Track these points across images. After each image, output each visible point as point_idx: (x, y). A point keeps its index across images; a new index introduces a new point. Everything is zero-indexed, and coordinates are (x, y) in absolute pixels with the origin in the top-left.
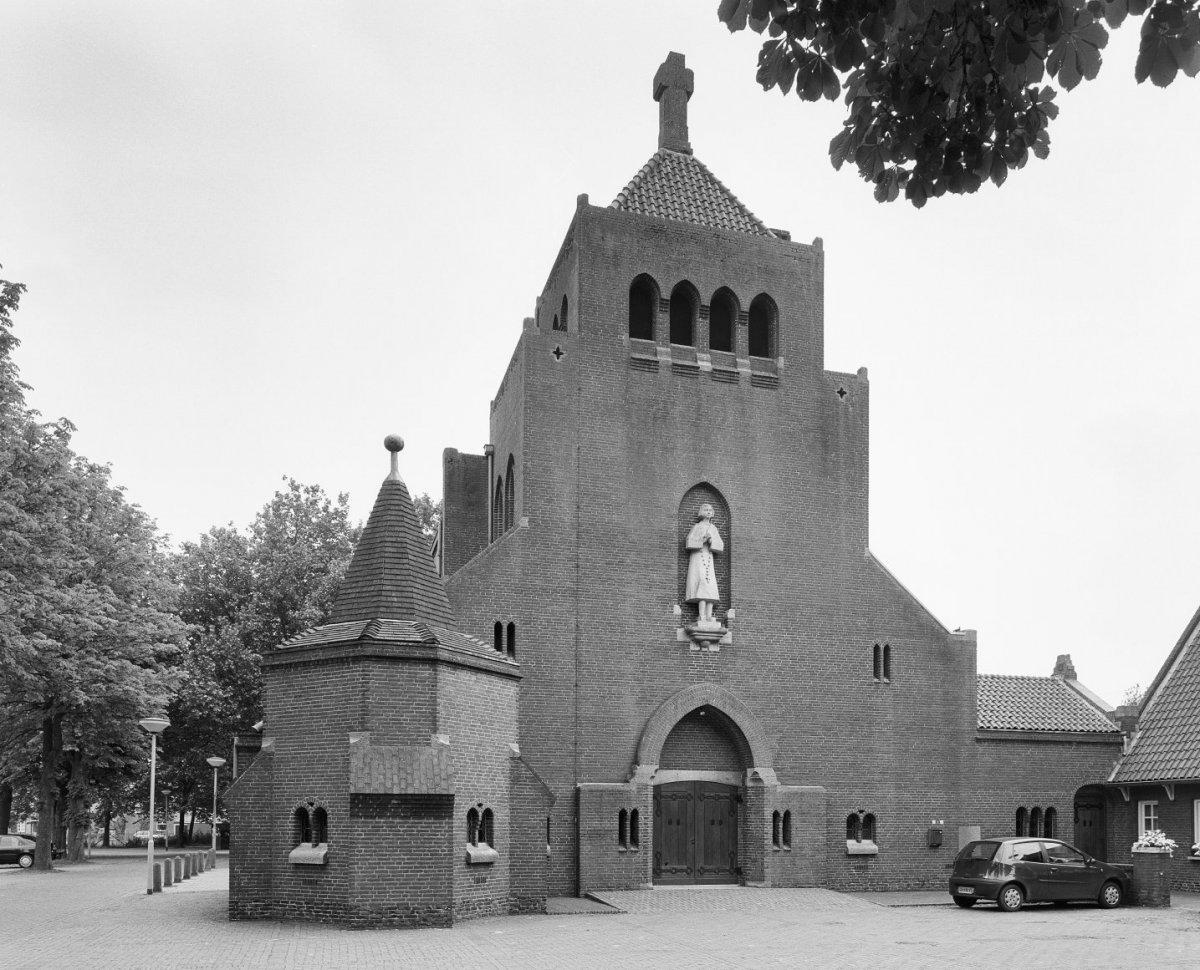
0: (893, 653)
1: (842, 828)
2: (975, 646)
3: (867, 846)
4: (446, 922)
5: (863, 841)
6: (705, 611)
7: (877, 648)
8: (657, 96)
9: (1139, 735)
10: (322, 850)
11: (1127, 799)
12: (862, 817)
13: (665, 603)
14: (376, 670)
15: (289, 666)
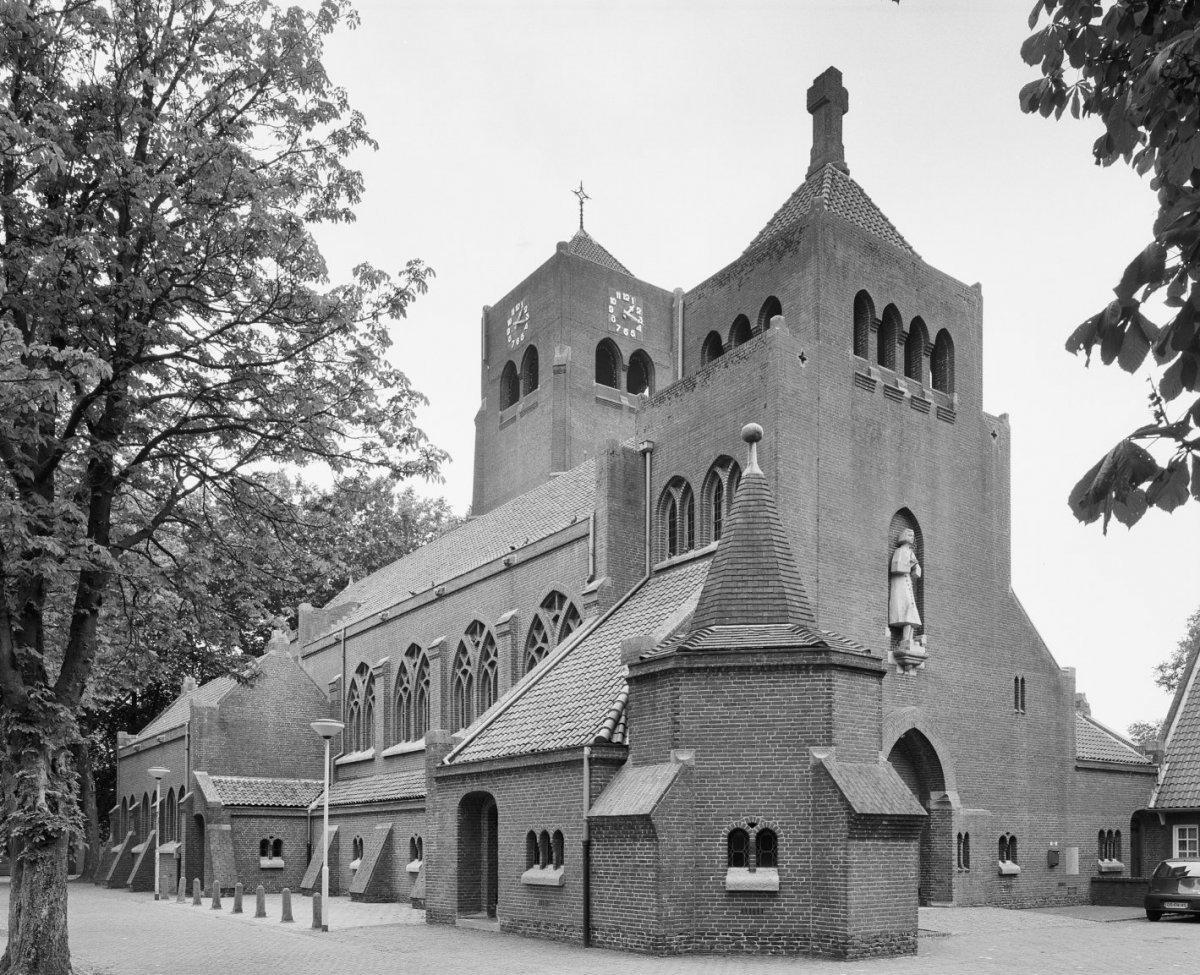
0: (1026, 685)
1: (720, 848)
2: (1074, 682)
4: (912, 949)
6: (908, 633)
7: (1016, 680)
8: (812, 109)
9: (1167, 766)
10: (561, 871)
11: (1163, 823)
12: (753, 833)
13: (879, 625)
14: (840, 681)
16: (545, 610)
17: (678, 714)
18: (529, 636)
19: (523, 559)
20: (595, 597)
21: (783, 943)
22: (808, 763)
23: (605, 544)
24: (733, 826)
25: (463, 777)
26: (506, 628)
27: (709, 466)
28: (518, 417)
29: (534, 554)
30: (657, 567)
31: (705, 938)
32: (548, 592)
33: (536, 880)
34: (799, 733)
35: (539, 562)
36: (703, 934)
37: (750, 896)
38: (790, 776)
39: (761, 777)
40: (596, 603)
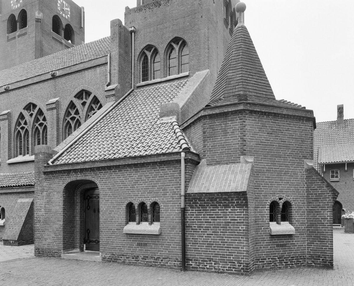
3: (154, 228)
5: (282, 223)
10: (4, 220)
15: (265, 113)
16: (26, 111)
17: (245, 136)
18: (66, 111)
19: (62, 74)
20: (113, 92)
21: (295, 262)
22: (304, 168)
23: (117, 68)
24: (272, 199)
25: (69, 171)
26: (54, 106)
27: (169, 41)
28: (17, 37)
29: (70, 72)
30: (138, 85)
31: (260, 262)
32: (79, 90)
33: (137, 231)
34: (300, 152)
35: (73, 76)
36: (259, 260)
37: (280, 237)
38: (296, 174)
39: (284, 173)
40: (114, 95)
